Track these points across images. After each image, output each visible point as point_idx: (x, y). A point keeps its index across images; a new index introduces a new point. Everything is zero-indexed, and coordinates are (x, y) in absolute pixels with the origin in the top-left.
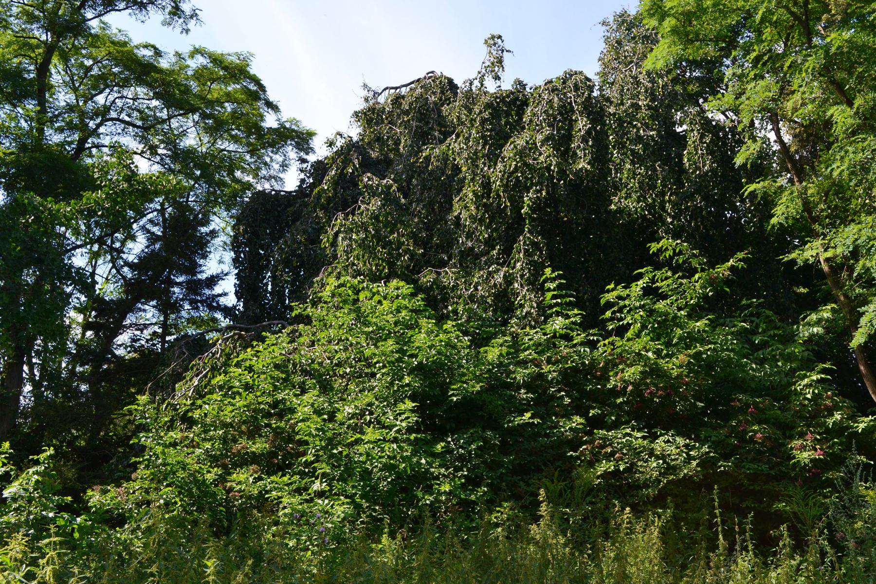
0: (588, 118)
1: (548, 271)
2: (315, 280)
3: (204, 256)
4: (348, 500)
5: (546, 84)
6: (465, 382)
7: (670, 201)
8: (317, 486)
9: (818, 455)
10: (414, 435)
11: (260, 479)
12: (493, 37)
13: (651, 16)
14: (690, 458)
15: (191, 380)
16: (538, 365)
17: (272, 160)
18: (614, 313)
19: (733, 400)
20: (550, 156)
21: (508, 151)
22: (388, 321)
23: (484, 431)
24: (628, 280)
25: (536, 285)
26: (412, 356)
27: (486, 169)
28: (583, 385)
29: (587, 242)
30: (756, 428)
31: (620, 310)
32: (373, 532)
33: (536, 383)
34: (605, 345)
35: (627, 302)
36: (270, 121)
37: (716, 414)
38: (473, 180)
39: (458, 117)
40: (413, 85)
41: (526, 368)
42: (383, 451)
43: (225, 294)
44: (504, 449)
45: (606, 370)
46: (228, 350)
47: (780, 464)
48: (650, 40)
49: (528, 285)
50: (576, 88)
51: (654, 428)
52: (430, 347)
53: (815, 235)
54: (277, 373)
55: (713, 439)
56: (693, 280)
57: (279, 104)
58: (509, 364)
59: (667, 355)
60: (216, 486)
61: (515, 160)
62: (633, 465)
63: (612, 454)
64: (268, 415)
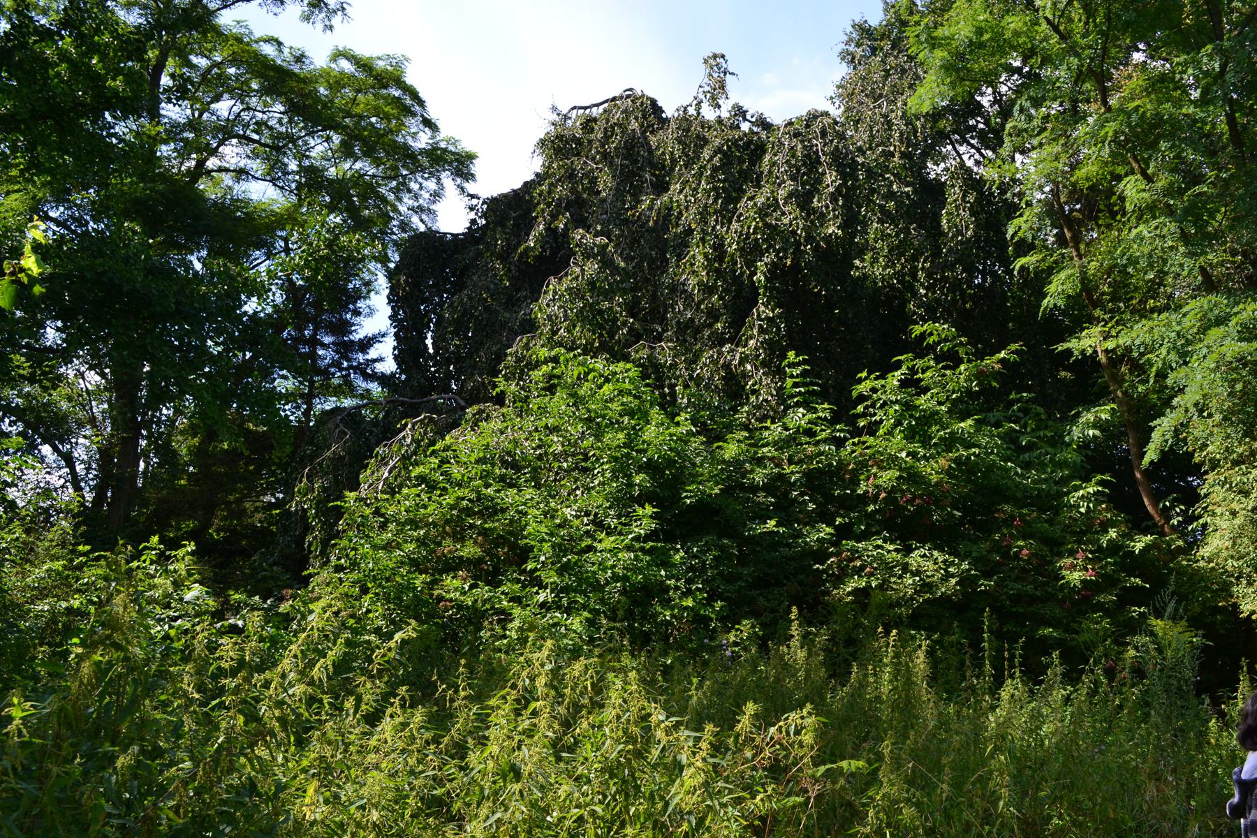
1: (791, 354)
2: (509, 351)
5: (786, 126)
6: (700, 483)
7: (923, 269)
9: (1090, 576)
12: (715, 56)
14: (948, 576)
17: (421, 188)
18: (866, 408)
19: (998, 511)
20: (796, 219)
24: (886, 368)
28: (830, 488)
29: (839, 326)
30: (1021, 543)
33: (777, 484)
34: (854, 444)
36: (422, 140)
37: (980, 527)
38: (703, 240)
40: (606, 105)
43: (380, 359)
47: (1047, 584)
50: (824, 133)
53: (1092, 321)
55: (974, 554)
63: (862, 568)
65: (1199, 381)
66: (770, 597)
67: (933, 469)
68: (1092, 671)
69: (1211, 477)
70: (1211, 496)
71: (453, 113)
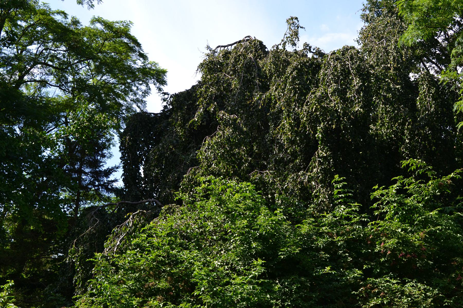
1: (337, 176)
5: (331, 55)
12: (292, 19)
14: (427, 297)
16: (331, 237)
17: (138, 89)
19: (453, 261)
21: (311, 98)
23: (300, 277)
24: (388, 184)
25: (327, 182)
26: (255, 230)
27: (296, 109)
28: (360, 249)
29: (362, 160)
33: (331, 247)
34: (372, 225)
39: (270, 70)
40: (235, 45)
43: (116, 181)
44: (312, 289)
45: (373, 241)
51: (404, 277)
55: (441, 285)
57: (147, 55)
62: (392, 300)
63: (379, 293)
67: (416, 238)
71: (156, 47)
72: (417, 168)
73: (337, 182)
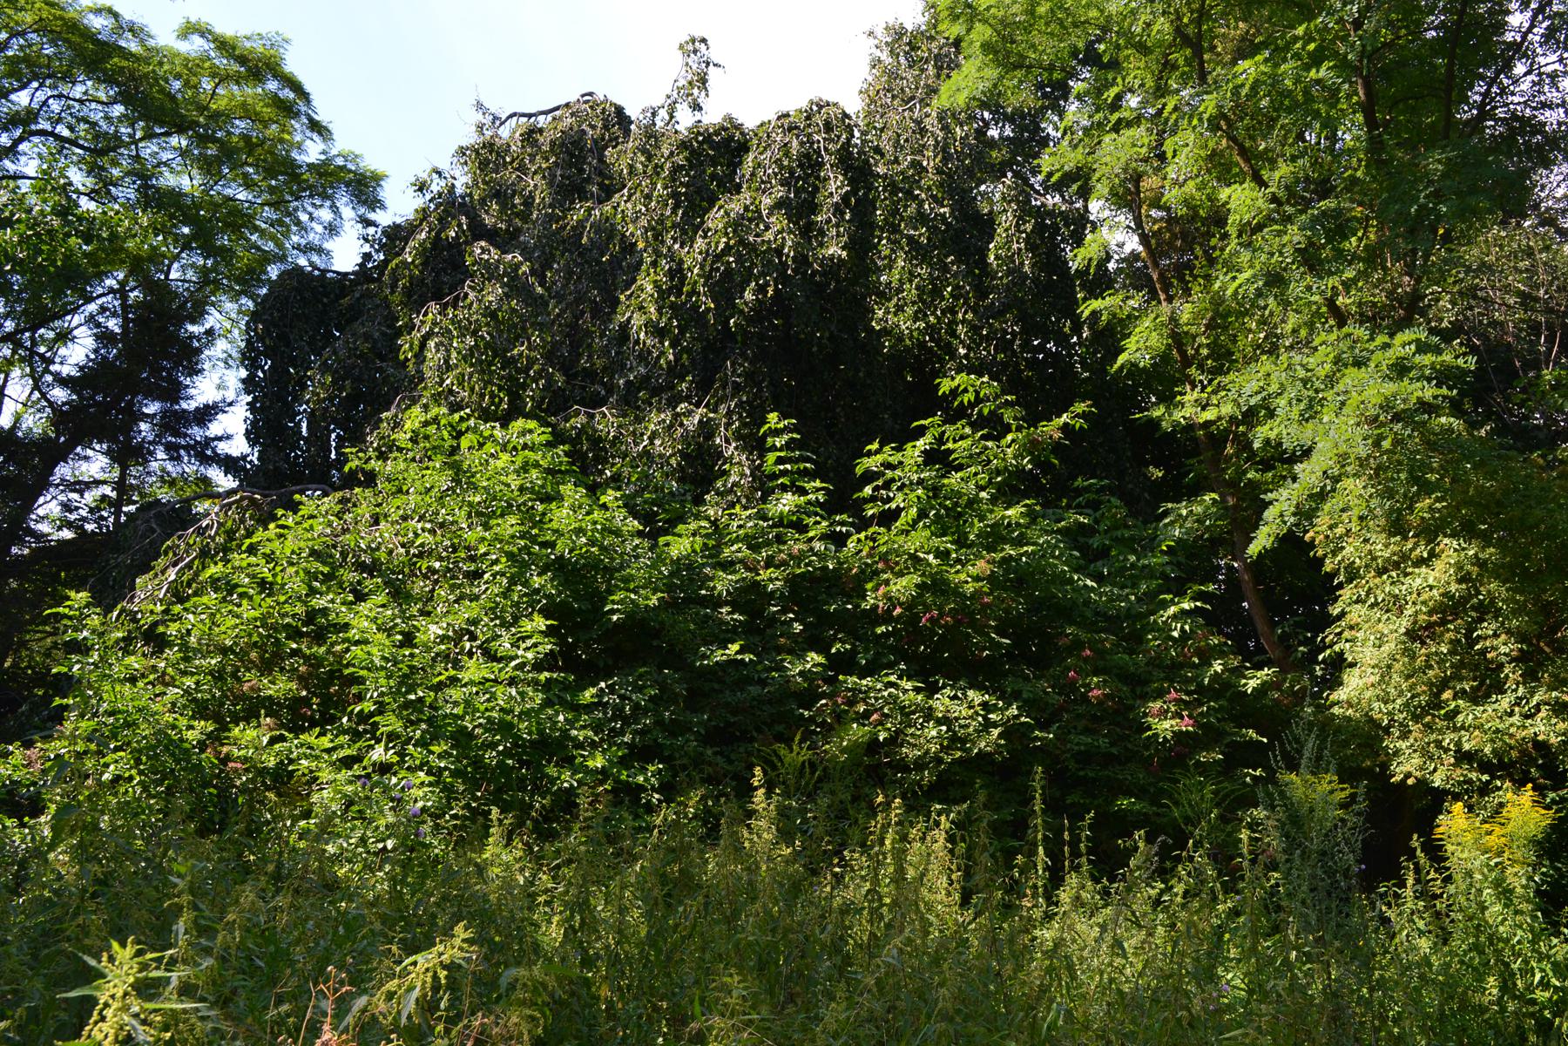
0: (845, 175)
1: (773, 417)
2: (384, 415)
3: (195, 371)
4: (431, 778)
5: (779, 118)
8: (378, 754)
9: (1186, 726)
10: (547, 674)
11: (282, 739)
13: (955, 18)
14: (988, 725)
15: (163, 572)
17: (312, 219)
18: (876, 489)
21: (715, 219)
22: (508, 485)
27: (677, 246)
28: (824, 599)
31: (887, 485)
32: (472, 832)
35: (898, 473)
36: (312, 152)
38: (654, 264)
41: (734, 572)
42: (493, 697)
46: (229, 523)
48: (946, 64)
49: (737, 440)
50: (828, 127)
52: (579, 531)
54: (317, 566)
55: (1025, 696)
56: (1003, 442)
57: (330, 127)
58: (704, 565)
59: (958, 561)
60: (202, 751)
61: (726, 234)
63: (867, 715)
64: (295, 634)
65: (1336, 436)
66: (733, 757)
67: (971, 574)
68: (1191, 859)
69: (1347, 593)
70: (1348, 617)
72: (978, 400)
73: (777, 433)
